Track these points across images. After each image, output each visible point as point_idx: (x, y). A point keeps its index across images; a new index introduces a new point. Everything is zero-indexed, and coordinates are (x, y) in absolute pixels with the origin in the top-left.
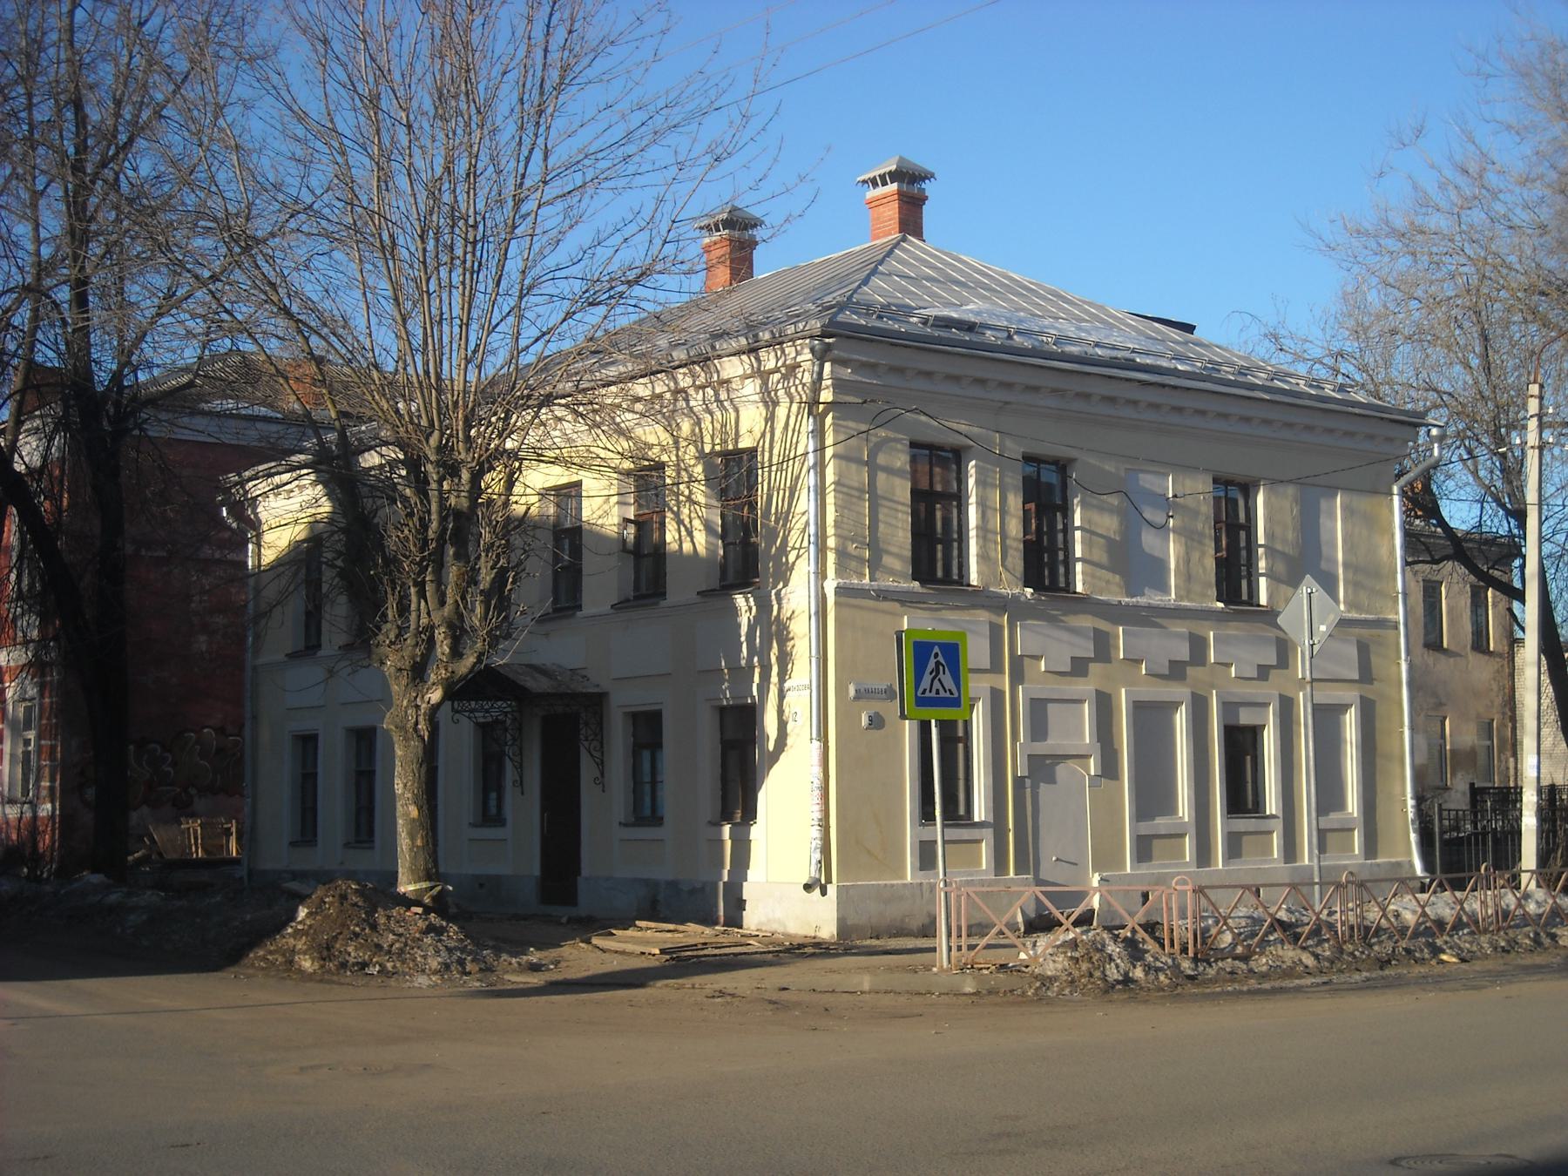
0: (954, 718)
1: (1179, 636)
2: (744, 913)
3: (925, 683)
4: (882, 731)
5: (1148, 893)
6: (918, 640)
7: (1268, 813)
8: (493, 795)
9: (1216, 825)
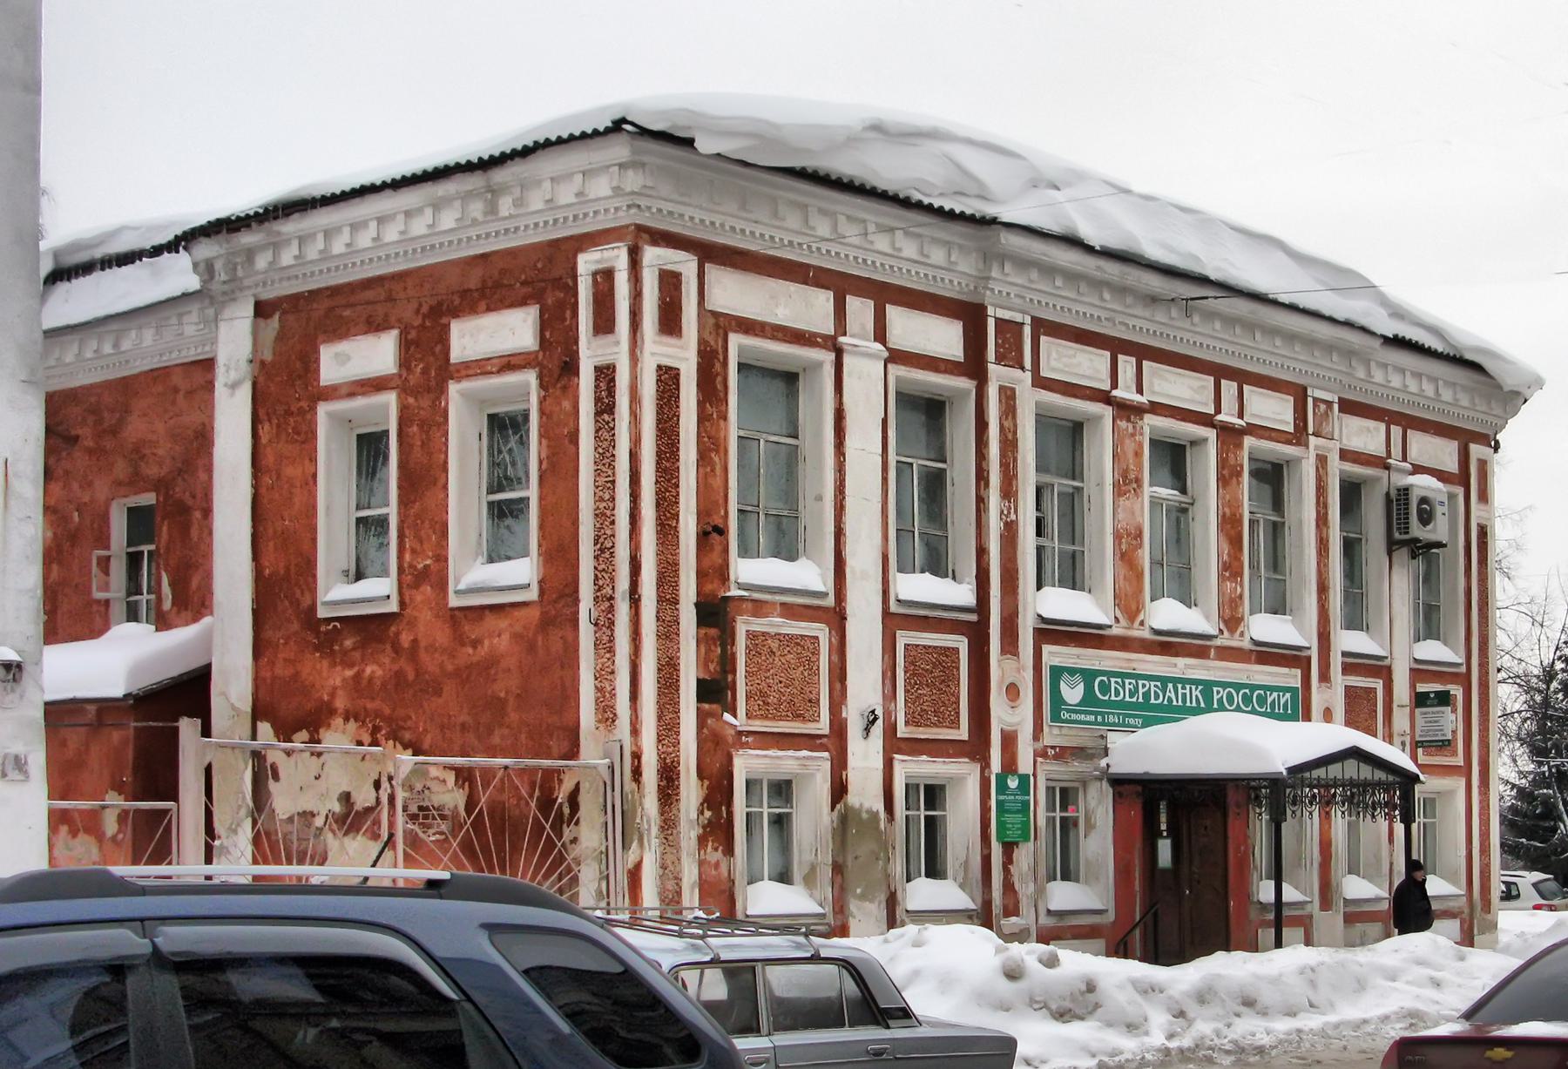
1: (1352, 830)
4: (336, 796)
9: (1272, 451)
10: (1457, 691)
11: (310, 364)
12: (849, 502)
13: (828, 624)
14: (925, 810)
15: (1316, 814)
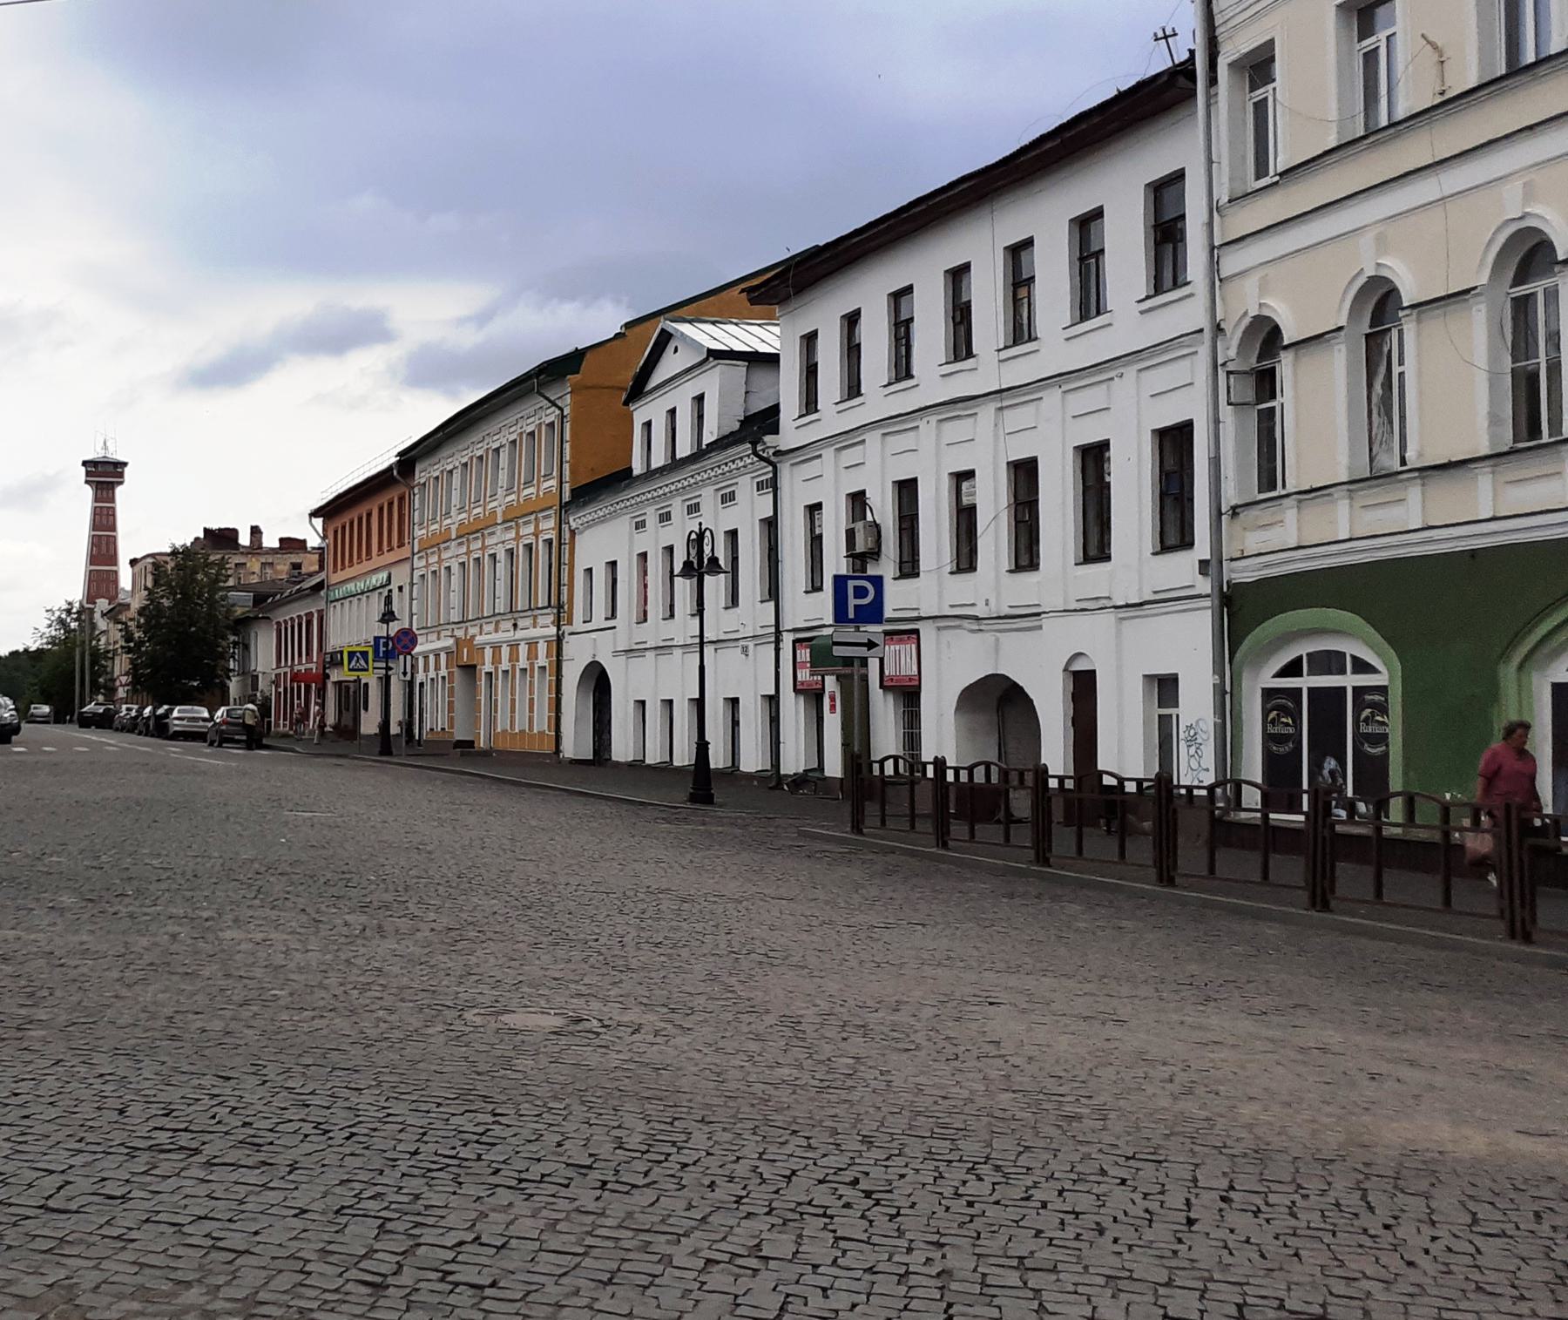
2: (119, 490)
5: (693, 799)
6: (215, 526)
7: (1539, 888)
12: (1456, 152)
14: (855, 597)
15: (145, 697)
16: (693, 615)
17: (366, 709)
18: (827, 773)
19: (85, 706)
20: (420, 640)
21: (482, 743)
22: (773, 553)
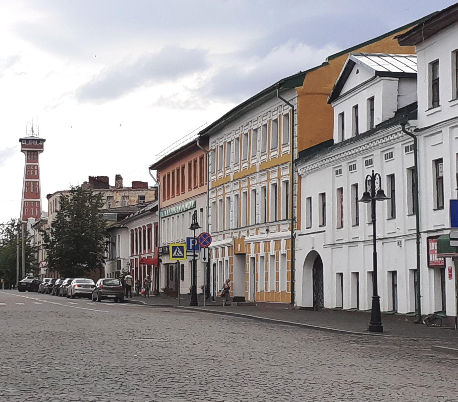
0: (115, 176)
3: (175, 253)
5: (371, 329)
8: (414, 182)
10: (186, 262)
11: (372, 312)
13: (440, 12)
16: (369, 224)
17: (183, 279)
18: (448, 314)
19: (22, 279)
20: (213, 239)
21: (249, 298)
22: (415, 187)
